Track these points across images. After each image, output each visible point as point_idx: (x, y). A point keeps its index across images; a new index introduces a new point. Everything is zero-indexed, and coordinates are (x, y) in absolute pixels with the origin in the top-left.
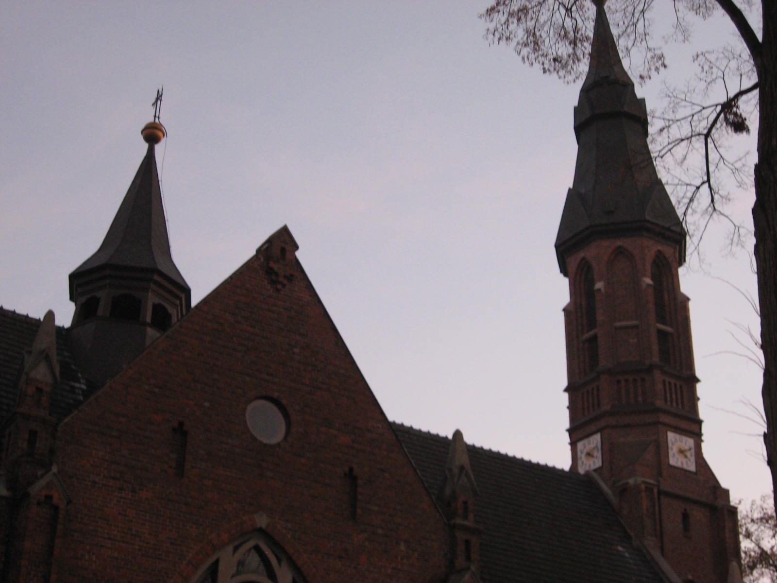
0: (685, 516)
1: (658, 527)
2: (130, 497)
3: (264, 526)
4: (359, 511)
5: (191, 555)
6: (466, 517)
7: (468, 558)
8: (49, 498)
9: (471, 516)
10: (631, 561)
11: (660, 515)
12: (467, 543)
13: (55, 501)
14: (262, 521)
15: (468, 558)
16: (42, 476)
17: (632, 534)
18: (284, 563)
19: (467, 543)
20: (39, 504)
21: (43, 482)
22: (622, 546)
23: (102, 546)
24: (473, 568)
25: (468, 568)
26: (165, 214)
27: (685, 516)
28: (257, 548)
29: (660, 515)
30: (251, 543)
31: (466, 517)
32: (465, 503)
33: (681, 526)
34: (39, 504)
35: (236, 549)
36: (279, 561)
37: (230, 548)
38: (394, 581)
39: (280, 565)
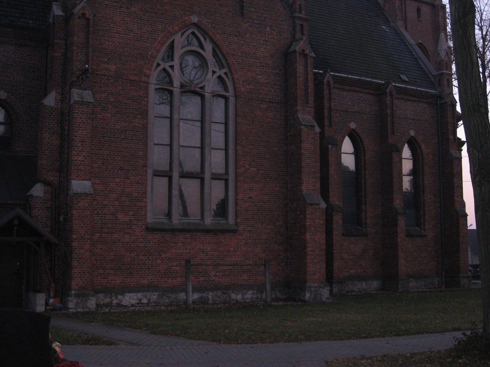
0: (419, 10)
1: (404, 16)
2: (126, 11)
3: (196, 22)
4: (245, 12)
5: (160, 39)
6: (301, 12)
7: (303, 34)
8: (84, 14)
9: (303, 12)
10: (387, 30)
11: (405, 10)
12: (302, 25)
13: (87, 16)
14: (195, 19)
15: (303, 34)
16: (79, 3)
17: (390, 20)
18: (208, 40)
19: (302, 25)
20: (79, 17)
21: (79, 7)
22: (385, 26)
23: (114, 37)
24: (304, 38)
25: (302, 39)
26: (224, 111)
27: (419, 10)
28: (193, 33)
29: (405, 10)
30: (190, 31)
31: (301, 12)
32: (300, 5)
33: (416, 15)
34: (79, 17)
35: (182, 34)
36: (205, 39)
37: (180, 34)
38: (414, 366)
39: (206, 42)
